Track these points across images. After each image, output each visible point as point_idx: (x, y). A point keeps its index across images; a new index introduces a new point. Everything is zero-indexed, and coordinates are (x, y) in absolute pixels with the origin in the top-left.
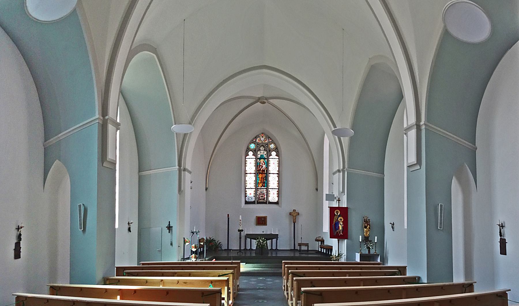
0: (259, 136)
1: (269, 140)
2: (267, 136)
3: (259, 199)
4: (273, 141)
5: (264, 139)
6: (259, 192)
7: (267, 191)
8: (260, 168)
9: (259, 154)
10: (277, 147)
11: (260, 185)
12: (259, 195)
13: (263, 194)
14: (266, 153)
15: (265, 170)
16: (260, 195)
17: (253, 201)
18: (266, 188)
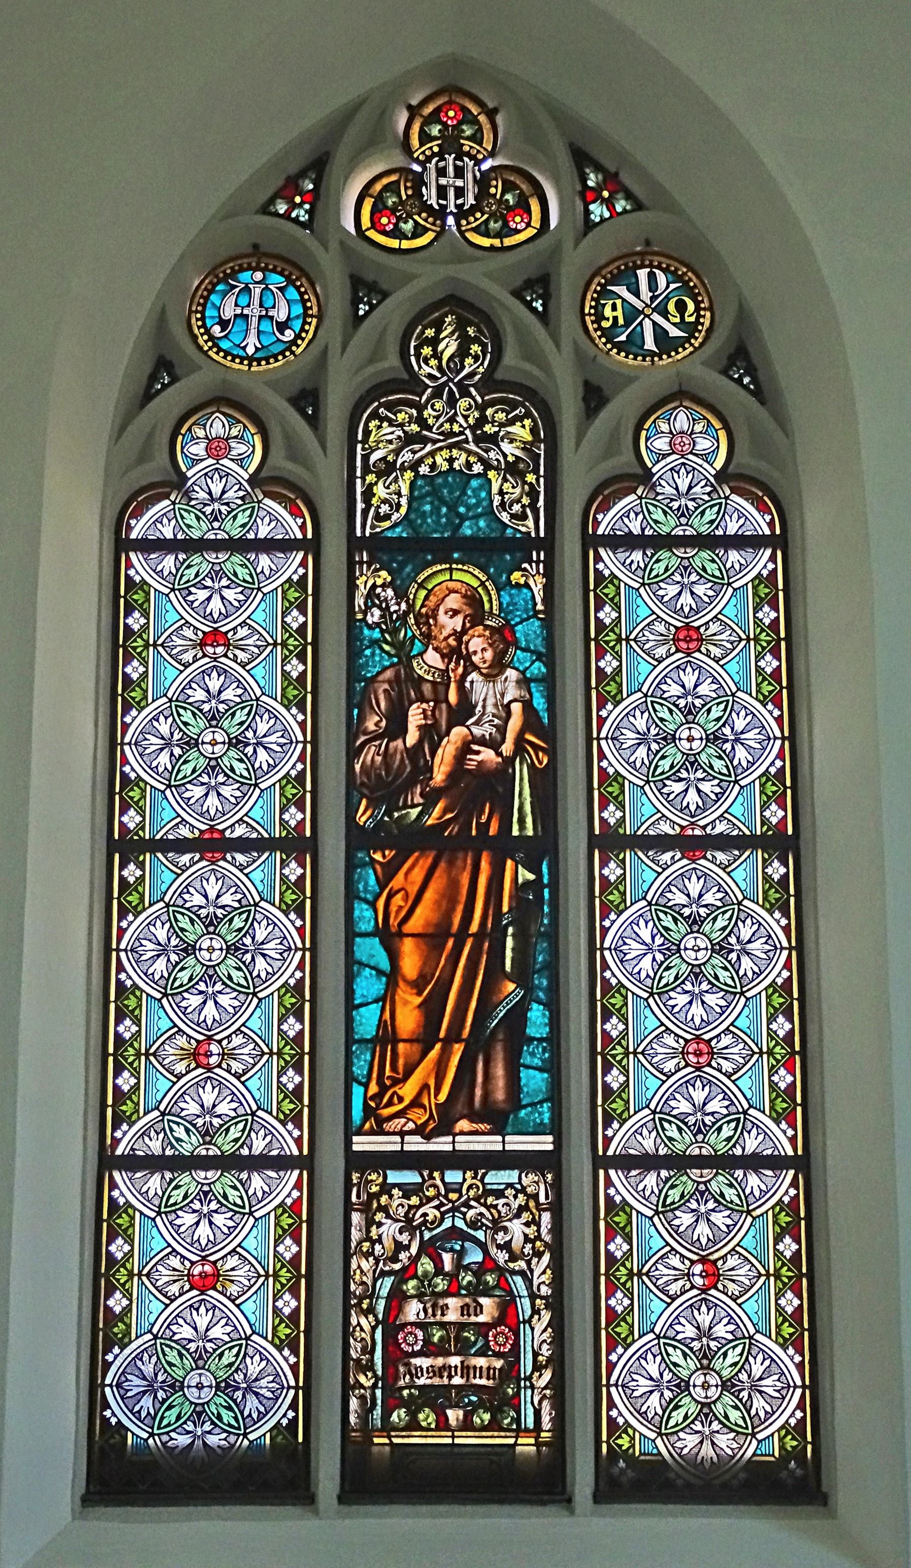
0: (384, 116)
1: (587, 195)
2: (544, 119)
3: (392, 1401)
4: (671, 207)
5: (483, 182)
6: (389, 1230)
7: (557, 1208)
8: (412, 737)
9: (387, 469)
10: (743, 316)
11: (408, 1090)
12: (397, 1298)
13: (478, 1290)
14: (521, 431)
15: (521, 773)
16: (413, 1310)
17: (261, 1433)
18: (545, 1143)
